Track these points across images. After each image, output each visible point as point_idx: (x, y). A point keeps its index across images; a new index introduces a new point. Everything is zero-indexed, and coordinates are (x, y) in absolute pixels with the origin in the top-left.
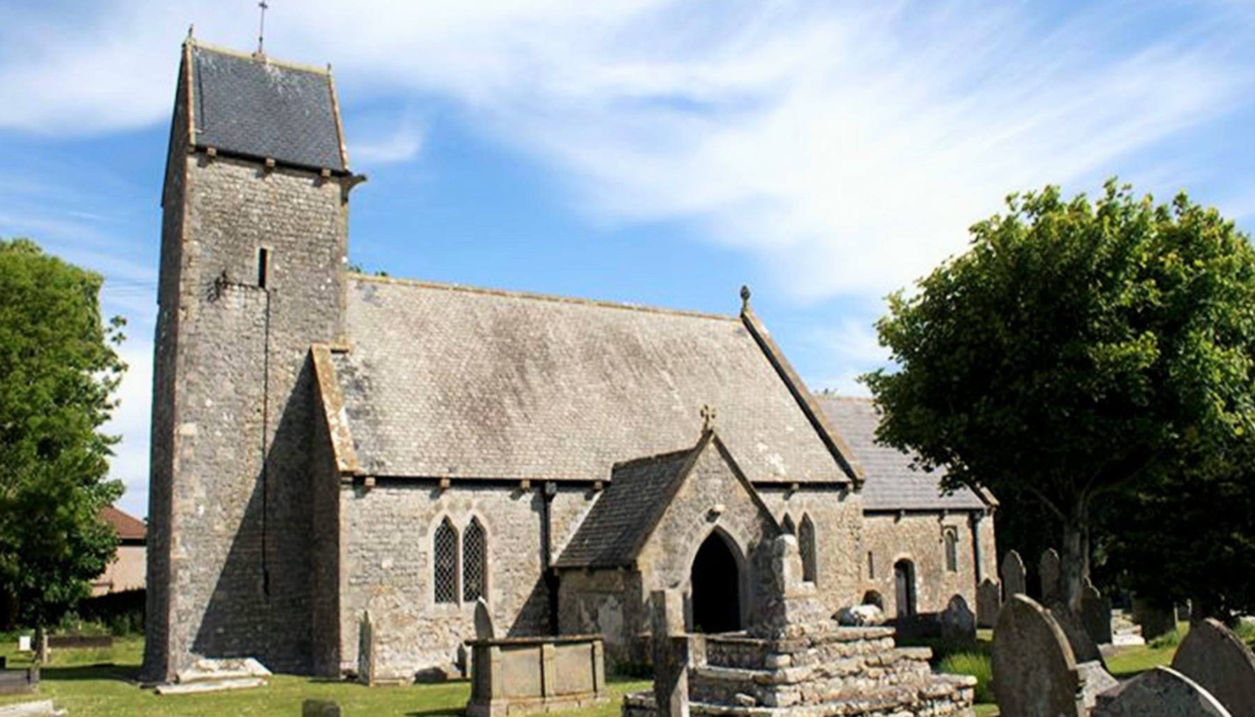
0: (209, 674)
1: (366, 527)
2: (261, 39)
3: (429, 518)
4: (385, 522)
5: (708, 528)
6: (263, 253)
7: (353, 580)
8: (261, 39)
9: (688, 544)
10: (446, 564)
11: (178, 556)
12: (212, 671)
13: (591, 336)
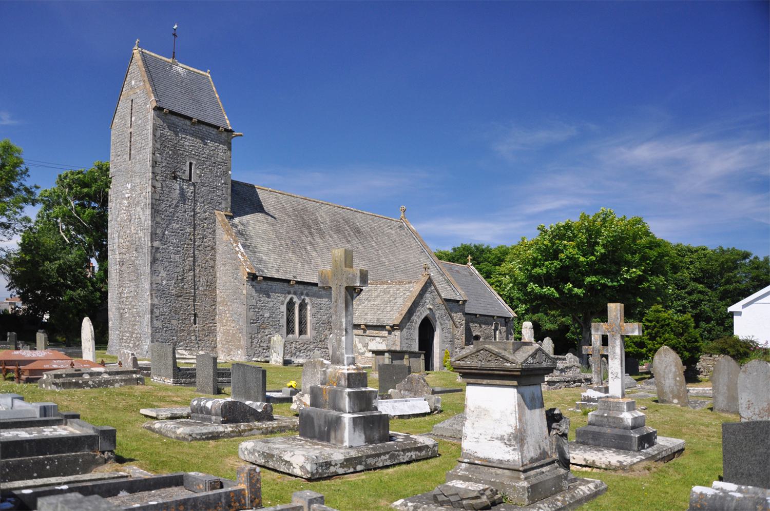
0: (184, 356)
2: (174, 53)
8: (174, 53)
13: (337, 221)
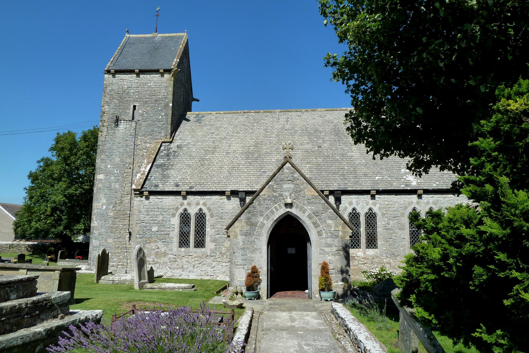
1: (146, 213)
3: (177, 209)
4: (154, 211)
5: (283, 211)
6: (135, 107)
7: (138, 236)
9: (265, 222)
10: (186, 229)
11: (94, 225)
12: (9, 262)
